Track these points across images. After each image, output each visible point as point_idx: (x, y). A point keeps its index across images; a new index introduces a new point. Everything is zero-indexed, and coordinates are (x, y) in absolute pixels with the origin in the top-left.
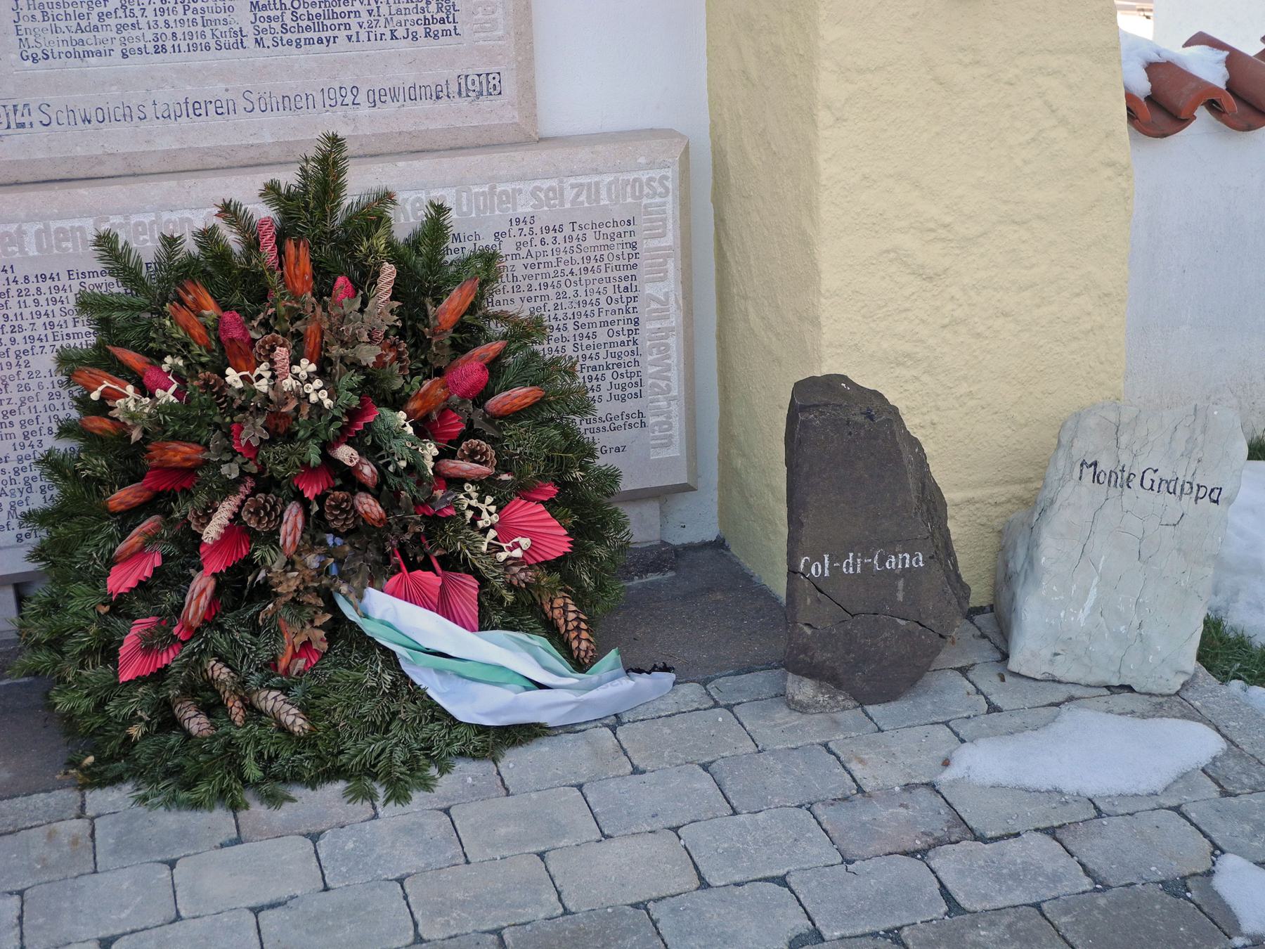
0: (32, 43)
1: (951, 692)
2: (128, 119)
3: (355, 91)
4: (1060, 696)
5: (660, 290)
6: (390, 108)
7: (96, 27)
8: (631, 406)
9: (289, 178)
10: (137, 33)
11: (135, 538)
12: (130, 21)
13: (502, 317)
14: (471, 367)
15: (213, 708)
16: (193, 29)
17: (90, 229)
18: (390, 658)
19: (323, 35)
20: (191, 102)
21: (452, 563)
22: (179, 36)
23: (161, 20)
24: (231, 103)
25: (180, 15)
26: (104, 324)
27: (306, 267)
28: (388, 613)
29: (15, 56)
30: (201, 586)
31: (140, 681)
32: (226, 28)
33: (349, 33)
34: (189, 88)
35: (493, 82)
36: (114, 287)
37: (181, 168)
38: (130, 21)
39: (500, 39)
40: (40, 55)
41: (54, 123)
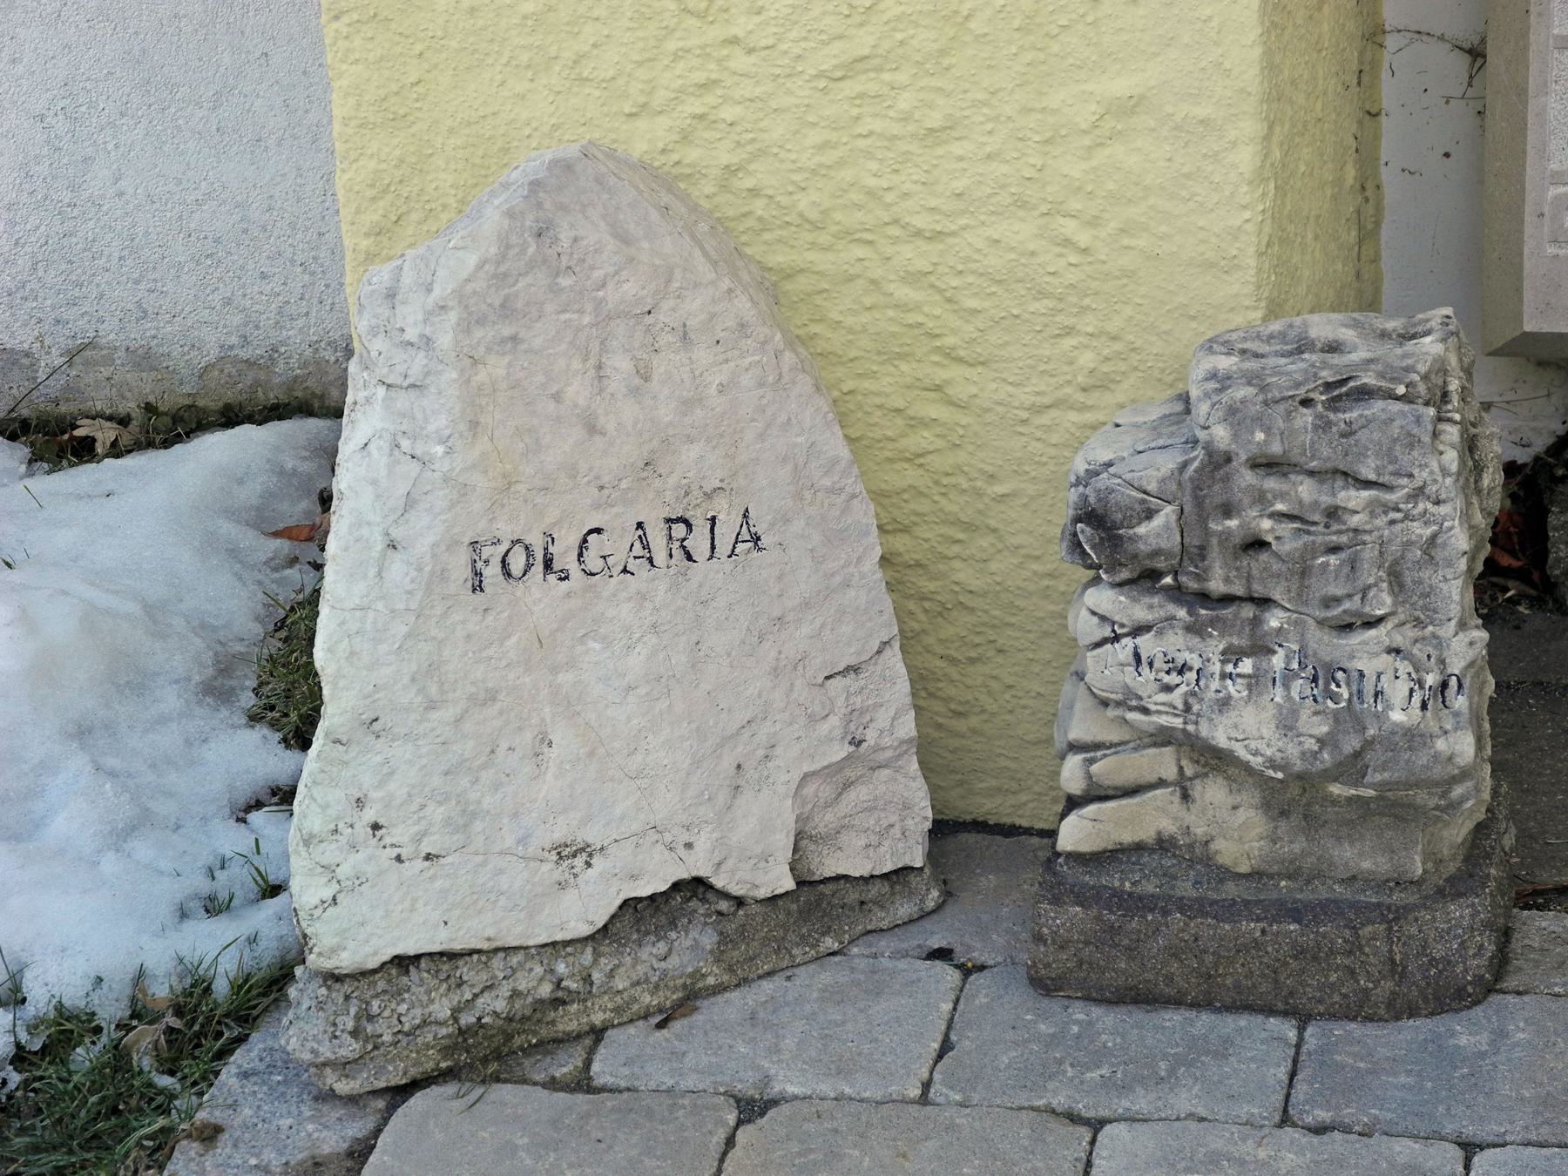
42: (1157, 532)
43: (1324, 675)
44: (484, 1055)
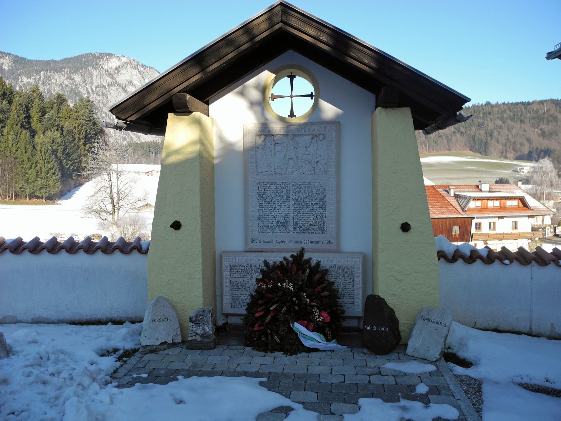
1: (394, 355)
4: (413, 358)
5: (358, 280)
8: (352, 300)
9: (295, 254)
11: (261, 309)
13: (328, 281)
14: (319, 288)
15: (267, 337)
17: (263, 259)
18: (297, 334)
21: (311, 321)
26: (263, 275)
27: (295, 269)
28: (298, 327)
30: (269, 317)
31: (256, 331)
36: (265, 268)
42: (194, 319)
43: (203, 328)
44: (152, 352)
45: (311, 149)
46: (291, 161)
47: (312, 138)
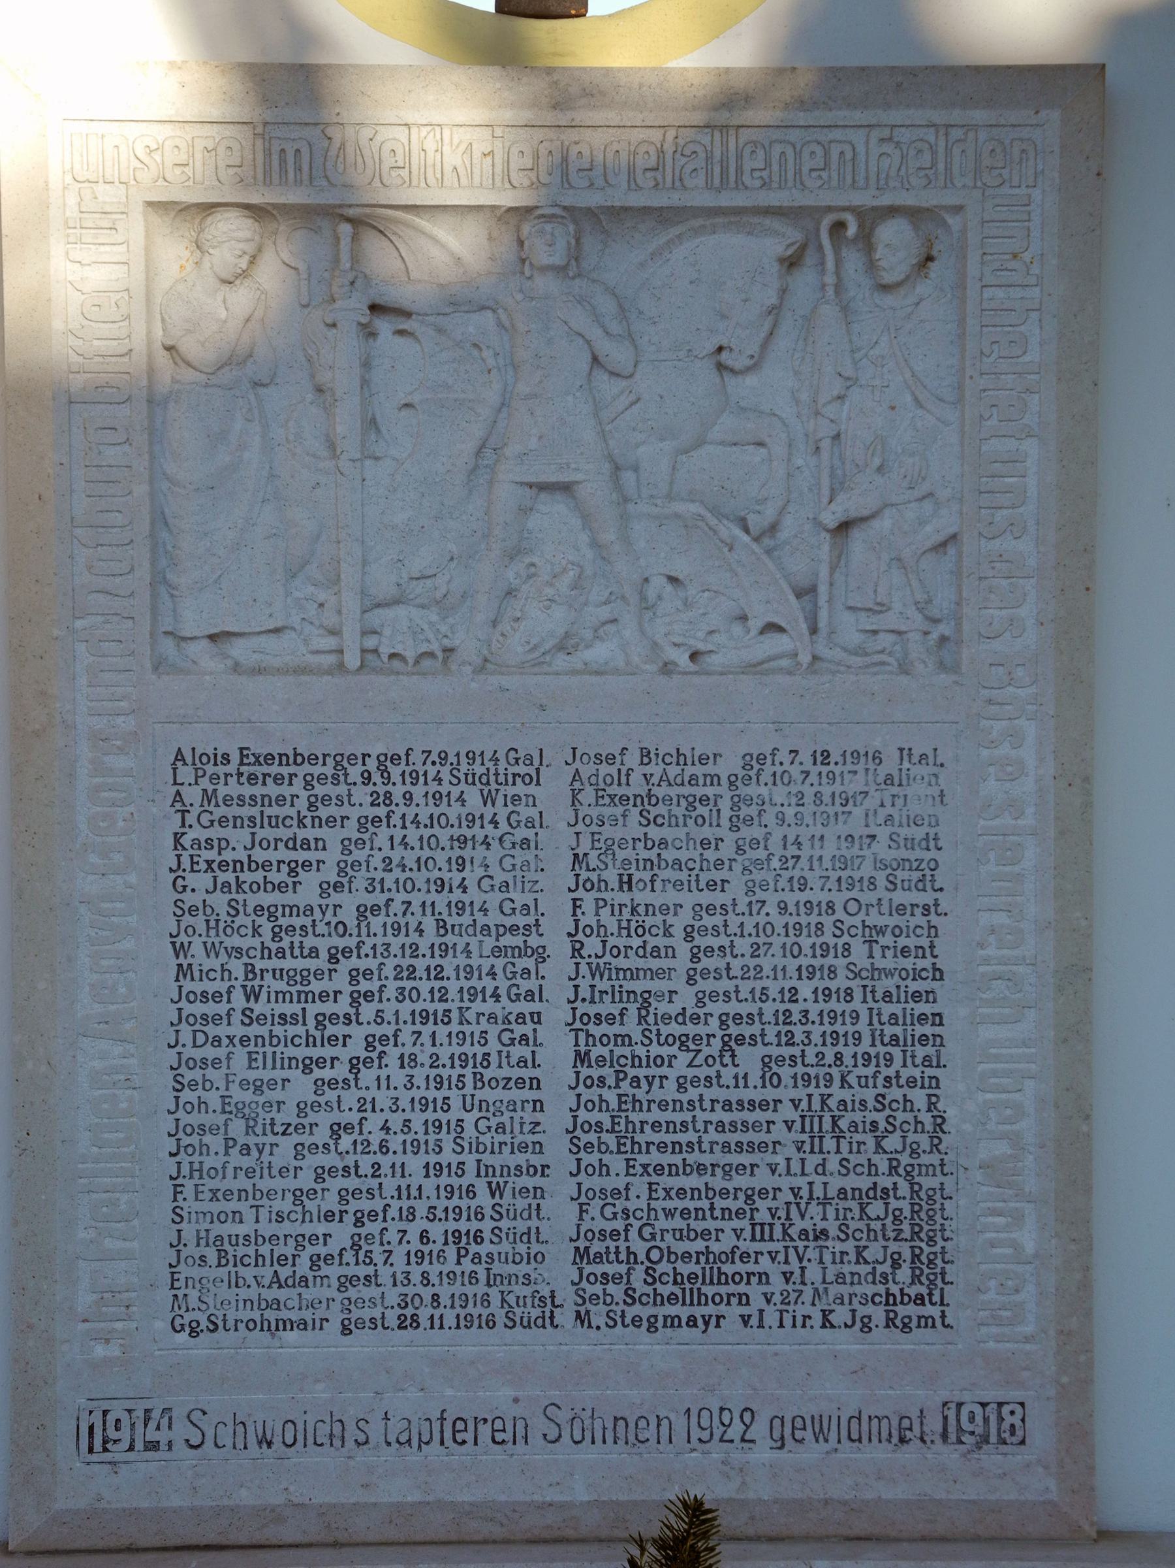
0: (193, 1302)
2: (337, 1442)
3: (747, 1417)
6: (811, 1452)
7: (304, 1280)
10: (374, 1291)
12: (362, 1271)
16: (470, 1290)
19: (698, 1311)
20: (450, 1417)
22: (445, 1300)
23: (416, 1272)
24: (520, 1425)
25: (451, 1265)
29: (162, 1325)
32: (527, 1291)
33: (745, 1310)
34: (449, 1392)
35: (1009, 1420)
37: (419, 1537)
38: (362, 1271)
39: (1027, 1339)
40: (204, 1324)
41: (209, 1443)
45: (773, 387)
46: (555, 509)
47: (791, 263)
